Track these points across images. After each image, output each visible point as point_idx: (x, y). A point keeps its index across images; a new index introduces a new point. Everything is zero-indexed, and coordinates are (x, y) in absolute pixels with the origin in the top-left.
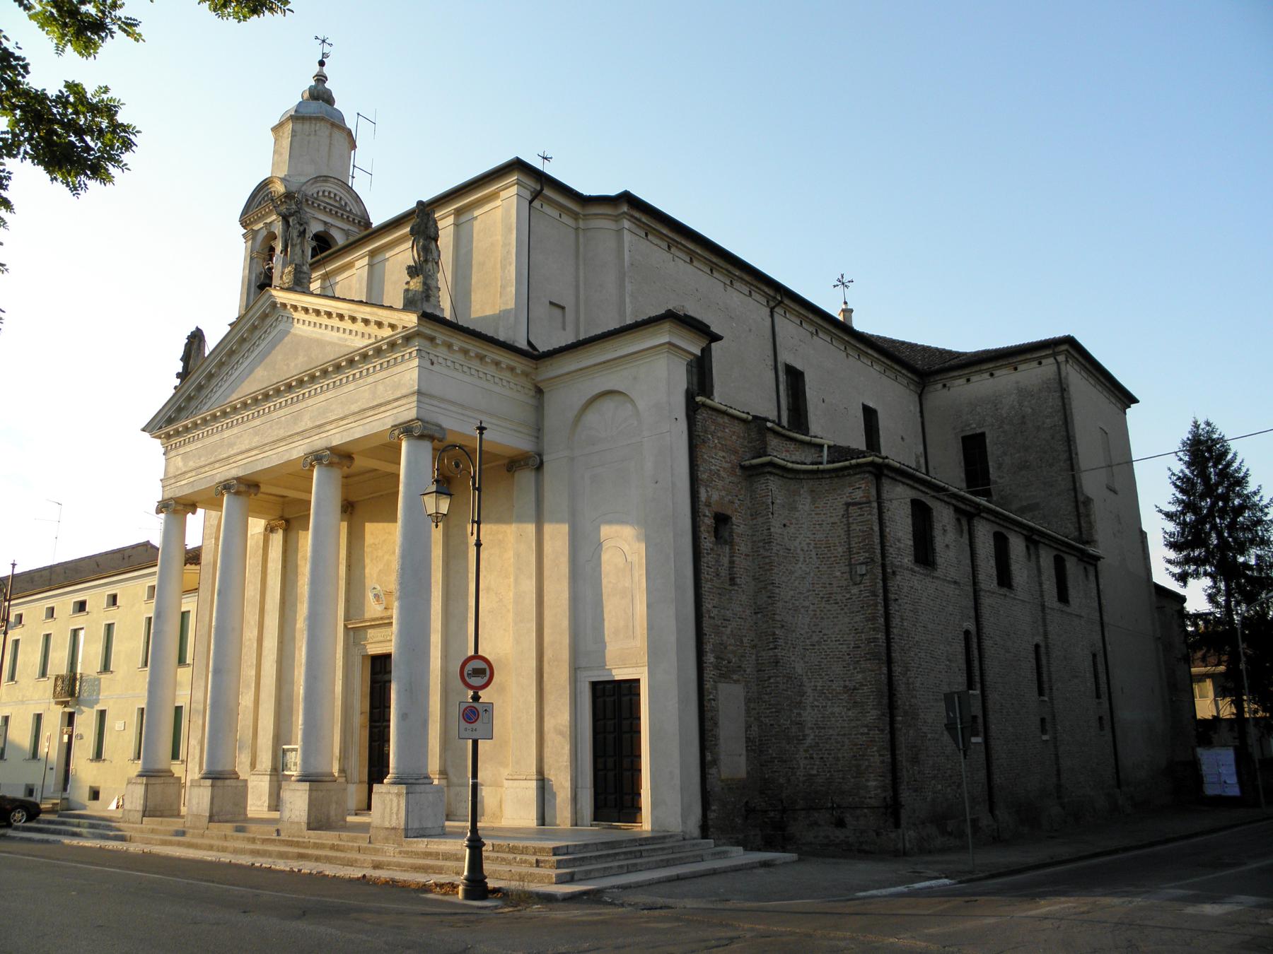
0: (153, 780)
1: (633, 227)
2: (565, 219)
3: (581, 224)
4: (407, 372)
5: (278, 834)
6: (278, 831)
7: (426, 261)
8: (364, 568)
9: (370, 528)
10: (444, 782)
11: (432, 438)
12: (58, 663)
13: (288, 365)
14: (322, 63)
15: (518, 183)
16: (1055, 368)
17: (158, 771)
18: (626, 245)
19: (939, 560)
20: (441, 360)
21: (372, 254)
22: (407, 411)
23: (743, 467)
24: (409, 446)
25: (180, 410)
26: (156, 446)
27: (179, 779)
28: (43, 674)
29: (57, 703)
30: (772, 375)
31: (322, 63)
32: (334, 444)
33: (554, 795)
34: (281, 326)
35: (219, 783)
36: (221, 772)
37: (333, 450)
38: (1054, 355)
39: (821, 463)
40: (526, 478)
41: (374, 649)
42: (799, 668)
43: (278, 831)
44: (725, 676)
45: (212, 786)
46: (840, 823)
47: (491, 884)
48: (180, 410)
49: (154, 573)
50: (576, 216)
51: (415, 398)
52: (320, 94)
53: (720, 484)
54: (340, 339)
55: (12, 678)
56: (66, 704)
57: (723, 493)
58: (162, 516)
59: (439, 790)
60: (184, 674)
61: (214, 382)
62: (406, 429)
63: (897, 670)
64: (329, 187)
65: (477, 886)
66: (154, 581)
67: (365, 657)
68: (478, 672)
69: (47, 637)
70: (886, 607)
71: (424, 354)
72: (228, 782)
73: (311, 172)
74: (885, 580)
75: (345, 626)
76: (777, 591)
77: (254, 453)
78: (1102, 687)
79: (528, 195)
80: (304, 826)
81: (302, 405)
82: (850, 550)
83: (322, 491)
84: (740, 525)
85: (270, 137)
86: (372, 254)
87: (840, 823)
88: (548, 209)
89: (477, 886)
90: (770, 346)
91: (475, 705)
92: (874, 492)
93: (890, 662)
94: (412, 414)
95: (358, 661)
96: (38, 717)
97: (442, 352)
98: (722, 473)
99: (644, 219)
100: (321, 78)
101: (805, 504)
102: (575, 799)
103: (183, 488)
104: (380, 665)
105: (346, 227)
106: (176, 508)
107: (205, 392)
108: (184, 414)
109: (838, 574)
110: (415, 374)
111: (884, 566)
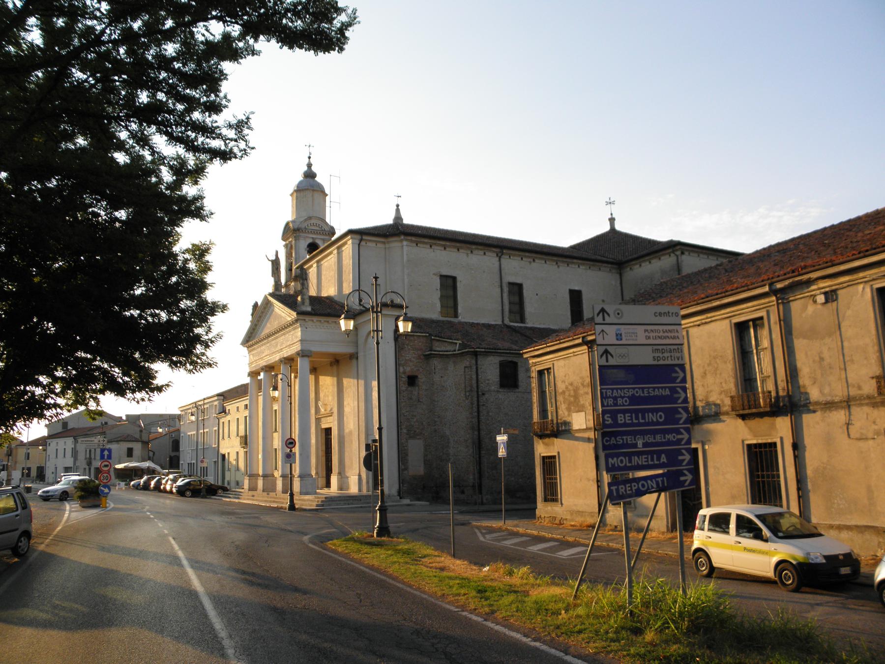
1: (409, 243)
2: (379, 245)
3: (387, 246)
9: (321, 378)
11: (308, 356)
12: (242, 433)
14: (309, 158)
16: (675, 258)
19: (520, 384)
21: (318, 262)
22: (297, 348)
25: (249, 337)
30: (499, 290)
31: (309, 158)
38: (673, 252)
40: (354, 361)
41: (324, 426)
42: (448, 433)
44: (413, 437)
46: (463, 492)
47: (297, 507)
50: (384, 243)
52: (310, 175)
53: (411, 364)
59: (315, 479)
62: (298, 354)
63: (483, 433)
65: (292, 507)
66: (247, 402)
67: (322, 429)
68: (291, 443)
70: (478, 408)
73: (305, 215)
74: (478, 397)
83: (302, 364)
84: (422, 379)
86: (318, 262)
87: (463, 492)
88: (369, 244)
89: (292, 507)
90: (498, 276)
93: (479, 430)
94: (299, 349)
97: (310, 323)
100: (309, 165)
101: (451, 367)
102: (368, 482)
103: (255, 367)
104: (328, 431)
105: (322, 237)
106: (253, 374)
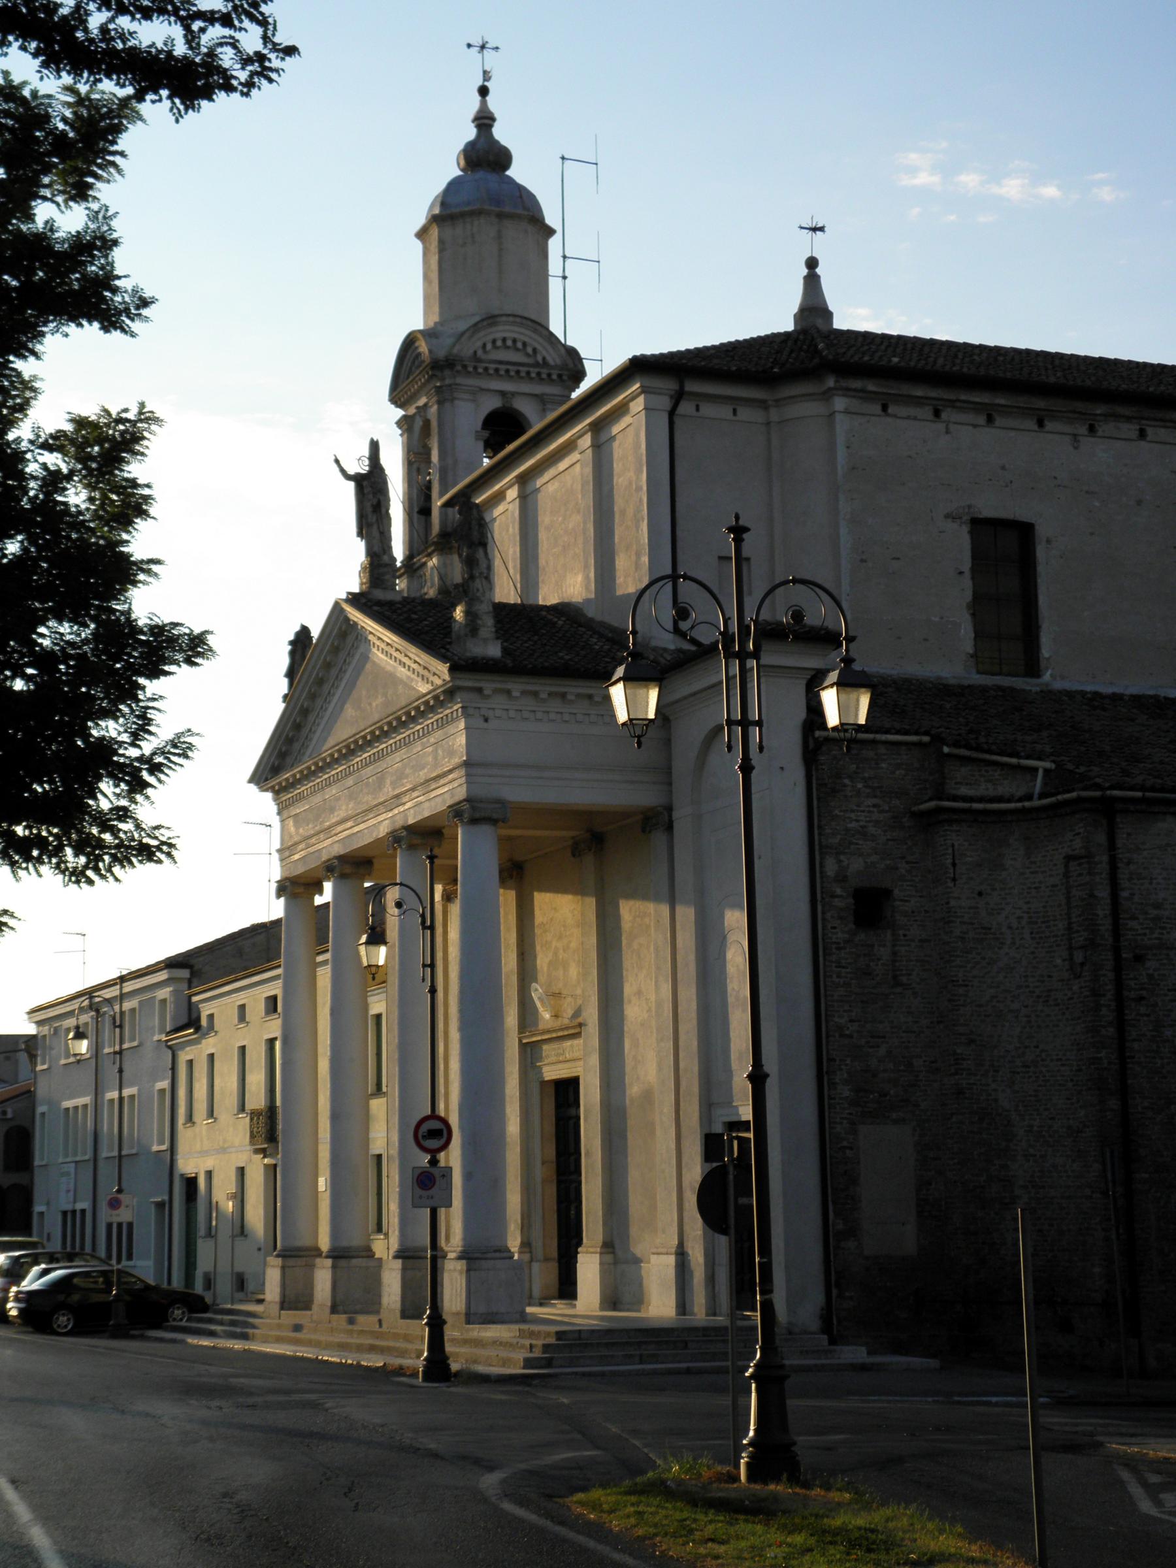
0: (291, 1262)
2: (745, 413)
3: (774, 415)
4: (455, 738)
5: (381, 1325)
6: (380, 1321)
7: (472, 577)
8: (535, 957)
10: (526, 1257)
13: (370, 704)
14: (483, 91)
15: (644, 390)
17: (299, 1249)
18: (841, 440)
20: (498, 713)
21: (523, 480)
23: (914, 815)
24: (463, 833)
25: (282, 755)
26: (264, 803)
27: (380, 1259)
28: (242, 1108)
29: (257, 1151)
31: (483, 91)
32: (411, 821)
33: (692, 1272)
34: (362, 649)
35: (343, 1263)
36: (348, 1249)
37: (410, 829)
39: (1029, 797)
40: (659, 838)
41: (552, 1072)
43: (380, 1321)
45: (334, 1267)
48: (282, 755)
49: (277, 977)
51: (462, 772)
52: (486, 157)
54: (409, 677)
55: (211, 1113)
56: (264, 1152)
57: (874, 858)
58: (282, 899)
59: (519, 1266)
60: (378, 1106)
61: (311, 718)
62: (456, 811)
64: (501, 331)
66: (276, 989)
68: (434, 1134)
69: (243, 1048)
71: (471, 711)
72: (354, 1261)
74: (1118, 969)
75: (520, 1041)
76: (961, 991)
77: (349, 824)
78: (240, 1197)
79: (665, 402)
80: (398, 1314)
81: (382, 765)
82: (1069, 928)
85: (418, 246)
88: (708, 410)
91: (432, 1170)
92: (1101, 838)
94: (461, 793)
95: (535, 1089)
96: (241, 1171)
97: (500, 701)
98: (872, 830)
99: (871, 387)
100: (484, 121)
102: (711, 1279)
106: (296, 888)
107: (305, 731)
108: (289, 760)
109: (1059, 961)
110: (461, 740)
111: (1117, 950)
